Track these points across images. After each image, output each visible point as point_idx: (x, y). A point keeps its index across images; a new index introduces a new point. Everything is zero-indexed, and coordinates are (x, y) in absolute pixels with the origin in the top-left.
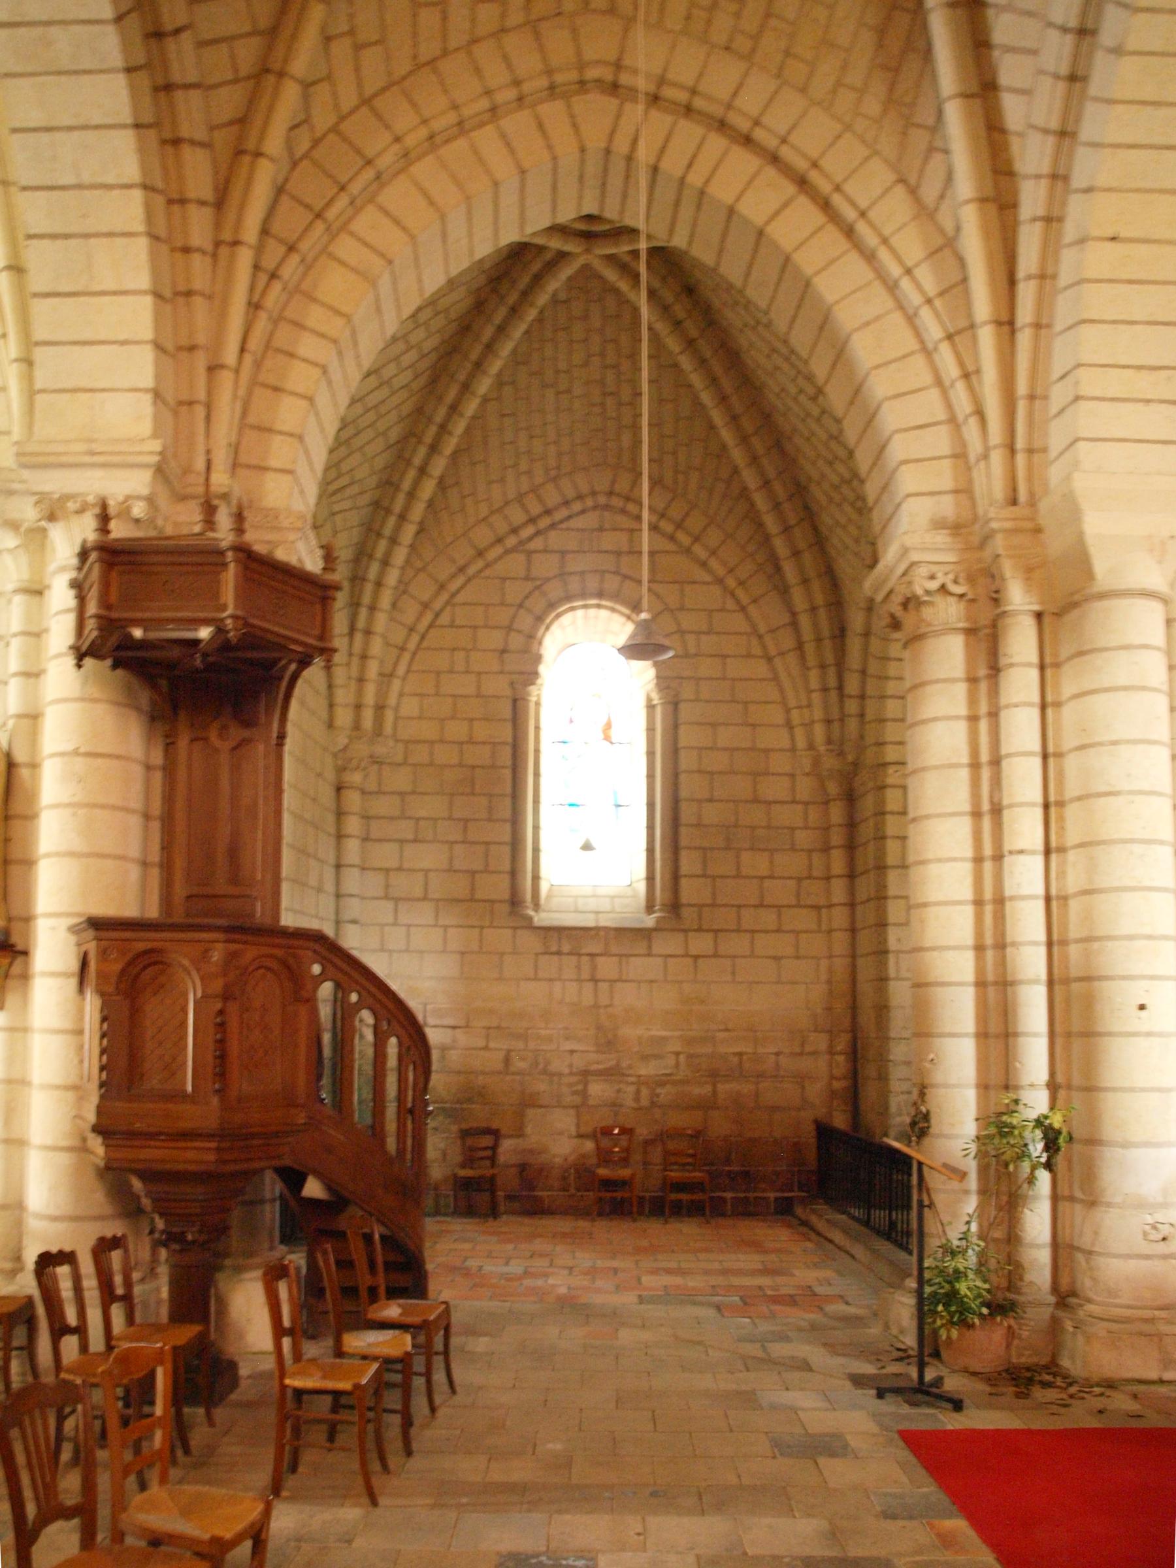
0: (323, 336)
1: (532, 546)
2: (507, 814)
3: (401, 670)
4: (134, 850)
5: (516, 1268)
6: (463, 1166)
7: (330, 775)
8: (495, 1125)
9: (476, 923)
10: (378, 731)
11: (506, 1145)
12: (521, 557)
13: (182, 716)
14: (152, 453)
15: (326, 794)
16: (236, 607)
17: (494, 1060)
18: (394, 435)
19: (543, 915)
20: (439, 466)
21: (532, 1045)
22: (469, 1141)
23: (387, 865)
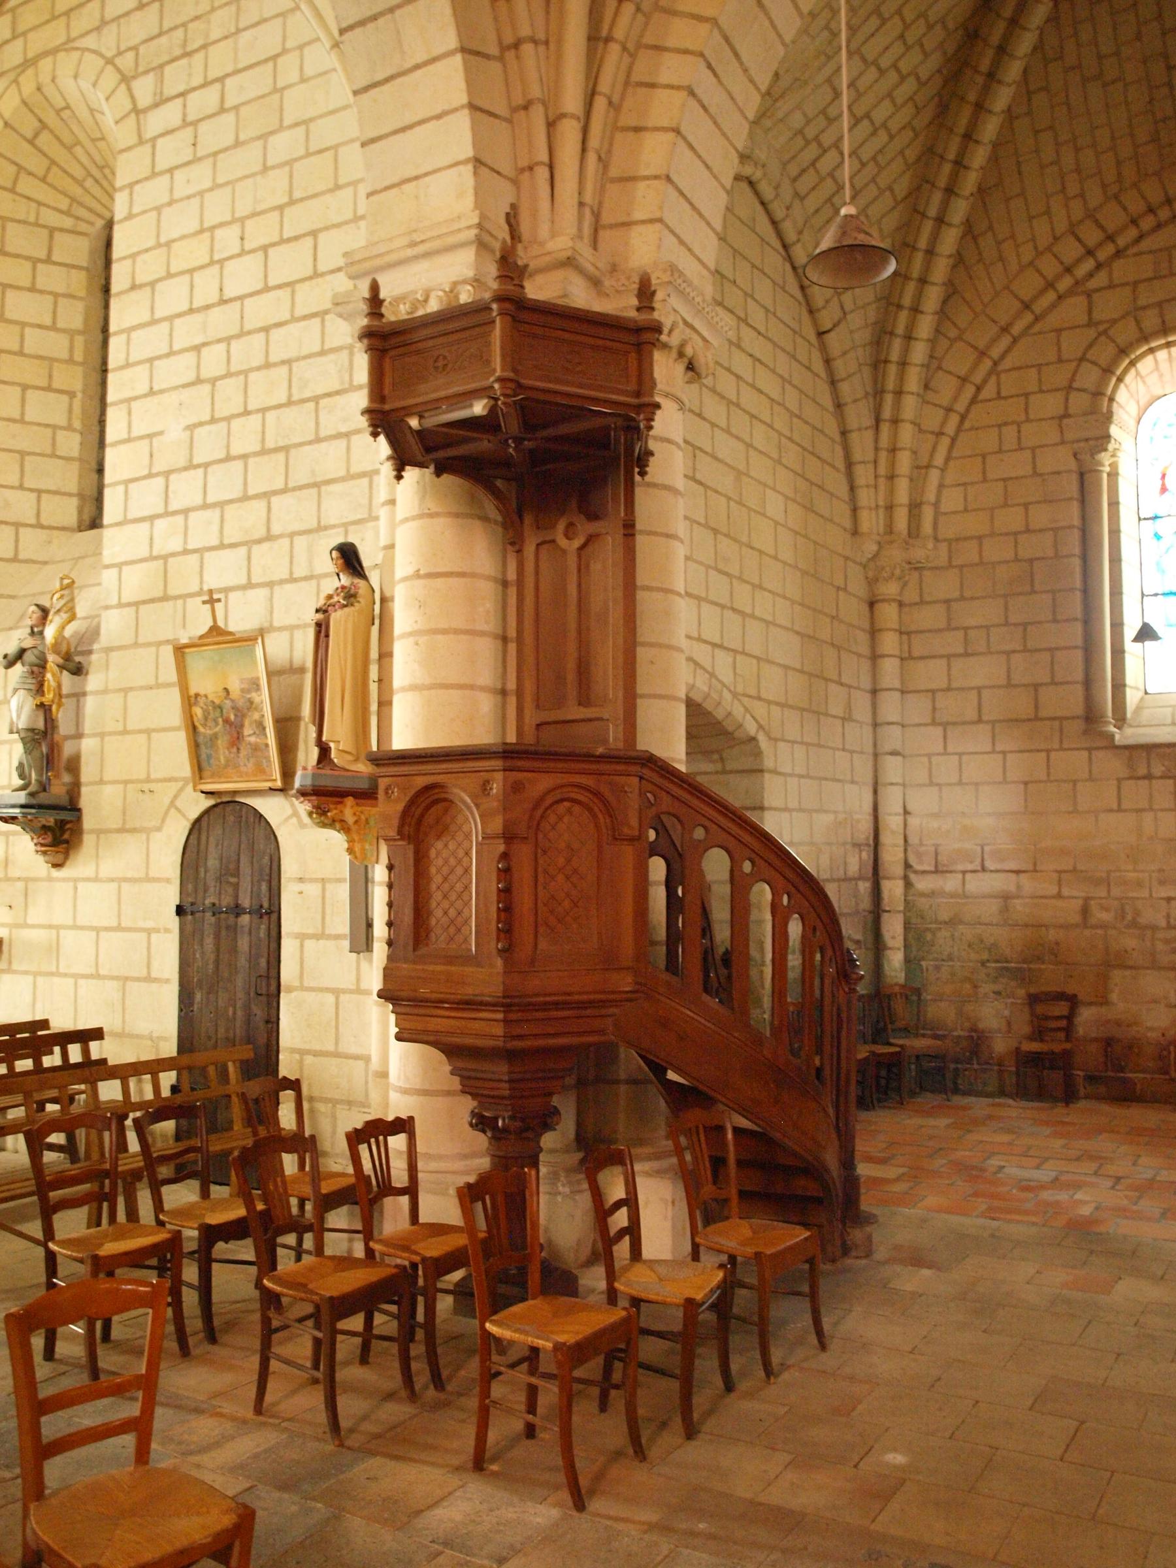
0: (686, 52)
1: (1092, 284)
2: (1078, 611)
3: (939, 460)
4: (486, 676)
5: (1044, 1175)
6: (1031, 1038)
7: (858, 587)
8: (1070, 989)
9: (1042, 746)
10: (914, 531)
11: (1086, 1015)
12: (1080, 301)
13: (528, 519)
14: (469, 227)
15: (853, 610)
16: (503, 370)
17: (1069, 910)
18: (901, 189)
19: (1128, 731)
20: (959, 210)
21: (1116, 891)
22: (1040, 1009)
23: (934, 686)
